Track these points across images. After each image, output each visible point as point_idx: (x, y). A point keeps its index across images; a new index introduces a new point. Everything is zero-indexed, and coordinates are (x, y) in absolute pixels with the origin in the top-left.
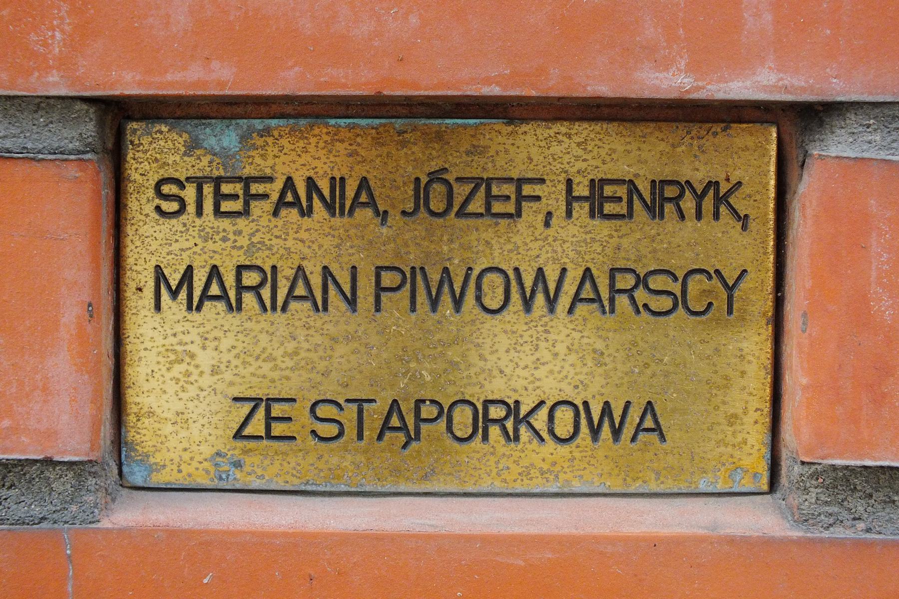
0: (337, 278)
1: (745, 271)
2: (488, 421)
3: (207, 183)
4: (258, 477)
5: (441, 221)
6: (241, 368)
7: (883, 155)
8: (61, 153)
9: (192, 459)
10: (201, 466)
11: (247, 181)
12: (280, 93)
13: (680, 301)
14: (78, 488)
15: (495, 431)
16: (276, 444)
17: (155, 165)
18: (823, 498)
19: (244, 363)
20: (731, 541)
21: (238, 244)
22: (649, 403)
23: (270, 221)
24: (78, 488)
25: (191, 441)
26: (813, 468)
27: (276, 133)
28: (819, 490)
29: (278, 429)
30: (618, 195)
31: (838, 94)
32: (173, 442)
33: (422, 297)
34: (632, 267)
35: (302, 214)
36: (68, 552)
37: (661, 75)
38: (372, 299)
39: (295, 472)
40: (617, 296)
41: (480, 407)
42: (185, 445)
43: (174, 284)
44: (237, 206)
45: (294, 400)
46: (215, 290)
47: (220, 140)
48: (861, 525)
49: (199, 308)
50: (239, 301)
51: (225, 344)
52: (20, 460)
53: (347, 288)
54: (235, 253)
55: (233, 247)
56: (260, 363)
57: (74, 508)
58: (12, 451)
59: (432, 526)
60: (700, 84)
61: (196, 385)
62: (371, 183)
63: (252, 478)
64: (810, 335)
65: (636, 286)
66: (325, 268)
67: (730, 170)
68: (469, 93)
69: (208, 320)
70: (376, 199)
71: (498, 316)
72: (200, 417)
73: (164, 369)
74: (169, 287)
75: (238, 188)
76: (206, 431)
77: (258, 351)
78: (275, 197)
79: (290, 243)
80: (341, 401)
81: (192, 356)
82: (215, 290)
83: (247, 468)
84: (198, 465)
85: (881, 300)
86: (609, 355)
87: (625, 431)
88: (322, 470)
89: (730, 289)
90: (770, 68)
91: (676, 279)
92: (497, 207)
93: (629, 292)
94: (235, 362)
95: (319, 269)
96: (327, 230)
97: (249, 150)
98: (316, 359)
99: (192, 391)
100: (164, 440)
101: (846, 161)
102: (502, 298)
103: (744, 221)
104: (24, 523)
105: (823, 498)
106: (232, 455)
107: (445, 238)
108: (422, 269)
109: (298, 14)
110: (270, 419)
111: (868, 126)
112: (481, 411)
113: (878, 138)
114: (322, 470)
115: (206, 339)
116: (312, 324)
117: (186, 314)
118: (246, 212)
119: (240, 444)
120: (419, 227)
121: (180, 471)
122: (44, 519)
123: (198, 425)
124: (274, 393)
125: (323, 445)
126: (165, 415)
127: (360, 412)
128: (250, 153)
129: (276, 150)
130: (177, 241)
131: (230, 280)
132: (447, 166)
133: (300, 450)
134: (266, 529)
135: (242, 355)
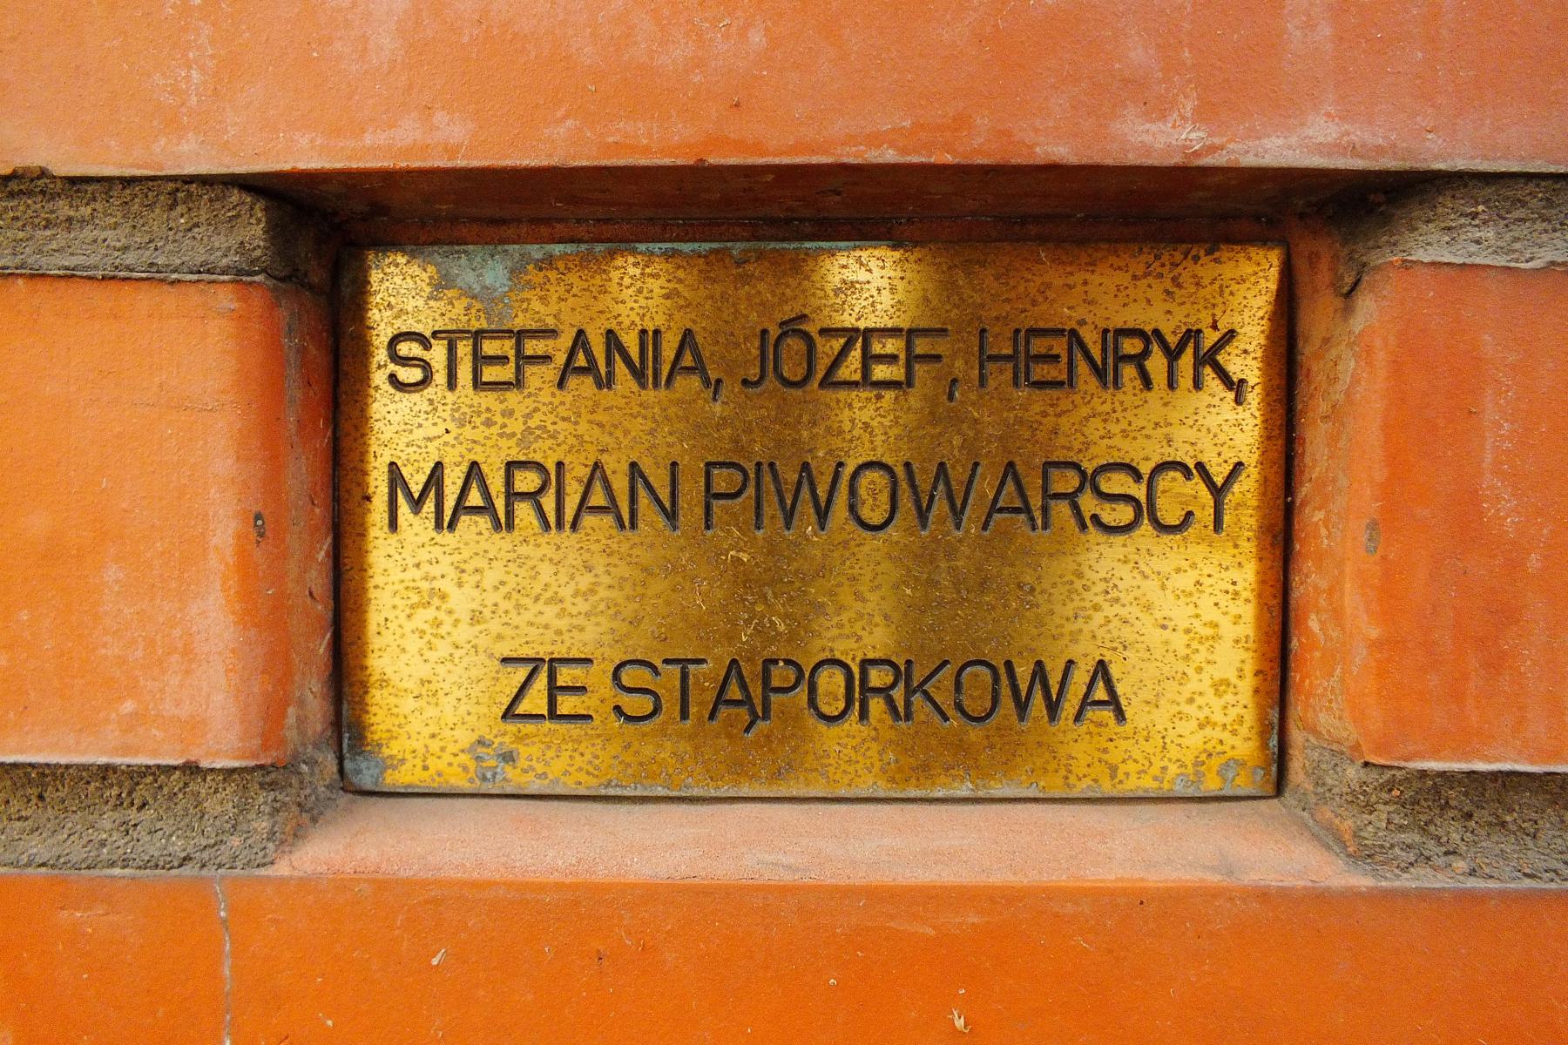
0: (651, 480)
1: (1240, 464)
2: (867, 690)
3: (462, 339)
4: (539, 776)
5: (798, 393)
6: (513, 614)
7: (1501, 261)
8: (208, 272)
9: (443, 749)
10: (456, 761)
11: (520, 336)
12: (545, 163)
13: (1145, 511)
14: (242, 809)
15: (877, 705)
16: (562, 728)
17: (389, 313)
18: (1397, 820)
19: (518, 606)
20: (1263, 895)
21: (508, 430)
22: (1101, 663)
23: (553, 395)
24: (242, 809)
25: (442, 723)
26: (1388, 775)
27: (561, 265)
28: (1391, 809)
29: (566, 704)
30: (1054, 352)
31: (1436, 158)
32: (416, 725)
33: (771, 508)
34: (1075, 459)
35: (599, 385)
36: (223, 914)
37: (1153, 127)
38: (699, 511)
39: (591, 770)
40: (1052, 503)
41: (856, 670)
42: (433, 729)
43: (416, 490)
44: (505, 373)
45: (588, 661)
46: (475, 498)
47: (481, 275)
48: (1461, 865)
49: (452, 526)
50: (510, 514)
51: (491, 578)
52: (148, 767)
53: (664, 495)
54: (504, 443)
55: (501, 435)
56: (540, 606)
57: (235, 841)
58: (137, 753)
59: (788, 867)
60: (1217, 141)
61: (449, 639)
62: (699, 339)
63: (530, 776)
64: (1384, 558)
65: (1080, 489)
66: (633, 465)
67: (1218, 312)
68: (845, 160)
69: (467, 544)
70: (706, 362)
71: (881, 534)
72: (455, 688)
73: (403, 616)
74: (409, 494)
75: (507, 347)
76: (463, 709)
77: (537, 589)
78: (561, 359)
79: (583, 428)
80: (658, 663)
81: (443, 597)
82: (475, 498)
83: (522, 763)
84: (452, 759)
85: (1498, 499)
86: (1042, 592)
87: (1067, 705)
88: (629, 765)
89: (1218, 492)
90: (1328, 115)
91: (1137, 476)
92: (881, 372)
93: (1072, 498)
94: (504, 605)
95: (625, 467)
96: (636, 409)
97: (522, 290)
98: (1106, 605)
99: (443, 649)
100: (403, 721)
101: (1447, 269)
102: (888, 507)
103: (1237, 388)
104: (157, 866)
105: (1397, 820)
106: (501, 744)
107: (805, 418)
108: (772, 465)
109: (570, 32)
110: (554, 690)
111: (1474, 216)
112: (857, 676)
113: (1491, 235)
114: (629, 765)
115: (463, 571)
116: (615, 547)
117: (434, 534)
118: (518, 383)
119: (512, 727)
120: (767, 404)
121: (425, 768)
122: (187, 859)
123: (451, 699)
124: (561, 651)
125: (631, 727)
126: (404, 685)
127: (684, 676)
128: (526, 295)
129: (562, 289)
130: (420, 426)
131: (496, 484)
132: (806, 312)
133: (599, 736)
134: (531, 878)
135: (515, 595)
